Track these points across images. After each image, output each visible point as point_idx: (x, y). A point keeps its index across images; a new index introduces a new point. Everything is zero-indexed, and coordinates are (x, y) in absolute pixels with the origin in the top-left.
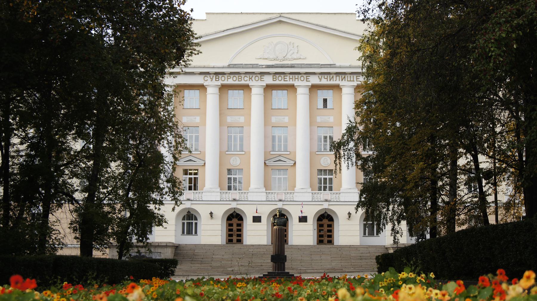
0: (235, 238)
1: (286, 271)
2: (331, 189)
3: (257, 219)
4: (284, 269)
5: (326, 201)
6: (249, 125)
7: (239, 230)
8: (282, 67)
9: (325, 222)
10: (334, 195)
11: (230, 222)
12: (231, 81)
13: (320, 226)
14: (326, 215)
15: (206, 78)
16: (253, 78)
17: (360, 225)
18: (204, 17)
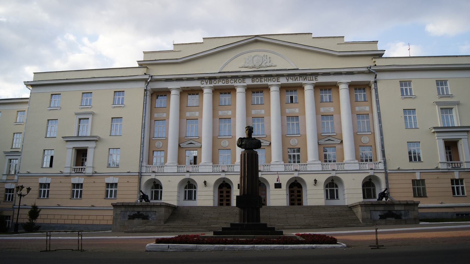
0: (225, 202)
1: (262, 221)
5: (296, 170)
6: (235, 117)
9: (296, 189)
10: (303, 167)
11: (221, 190)
12: (221, 84)
13: (221, 192)
16: (237, 81)
17: (286, 190)
18: (202, 41)
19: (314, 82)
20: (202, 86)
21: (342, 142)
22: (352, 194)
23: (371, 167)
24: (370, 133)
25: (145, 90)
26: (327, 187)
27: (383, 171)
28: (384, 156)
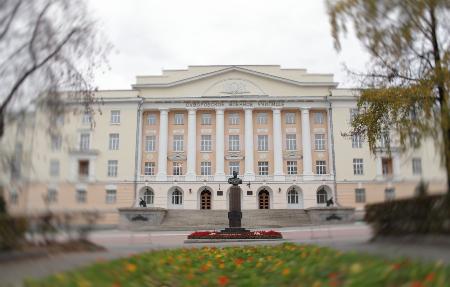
0: (206, 206)
1: (242, 227)
2: (267, 174)
3: (220, 193)
4: (240, 225)
5: (264, 181)
7: (261, 201)
8: (235, 97)
9: (206, 195)
10: (299, 177)
11: (203, 196)
12: (203, 107)
13: (261, 197)
14: (206, 190)
15: (188, 105)
16: (217, 105)
17: (168, 198)
18: (186, 68)
19: (281, 107)
20: (187, 108)
21: (302, 157)
22: (309, 200)
23: (324, 179)
24: (325, 150)
25: (139, 111)
26: (289, 194)
27: (333, 182)
28: (334, 169)
